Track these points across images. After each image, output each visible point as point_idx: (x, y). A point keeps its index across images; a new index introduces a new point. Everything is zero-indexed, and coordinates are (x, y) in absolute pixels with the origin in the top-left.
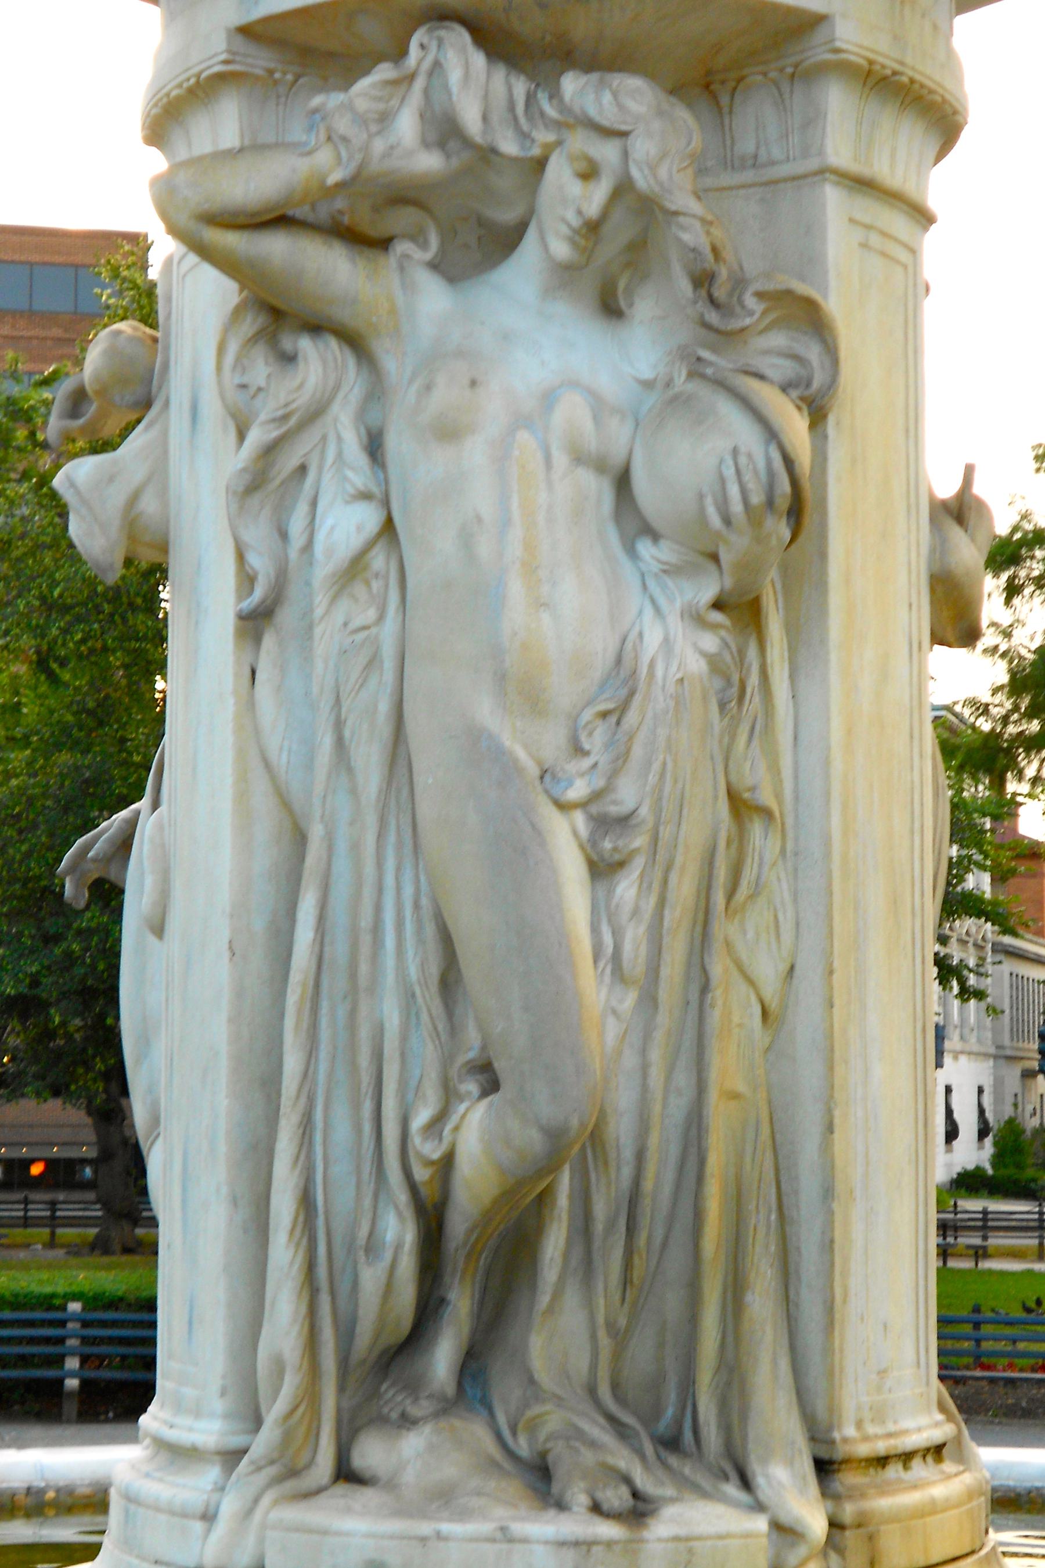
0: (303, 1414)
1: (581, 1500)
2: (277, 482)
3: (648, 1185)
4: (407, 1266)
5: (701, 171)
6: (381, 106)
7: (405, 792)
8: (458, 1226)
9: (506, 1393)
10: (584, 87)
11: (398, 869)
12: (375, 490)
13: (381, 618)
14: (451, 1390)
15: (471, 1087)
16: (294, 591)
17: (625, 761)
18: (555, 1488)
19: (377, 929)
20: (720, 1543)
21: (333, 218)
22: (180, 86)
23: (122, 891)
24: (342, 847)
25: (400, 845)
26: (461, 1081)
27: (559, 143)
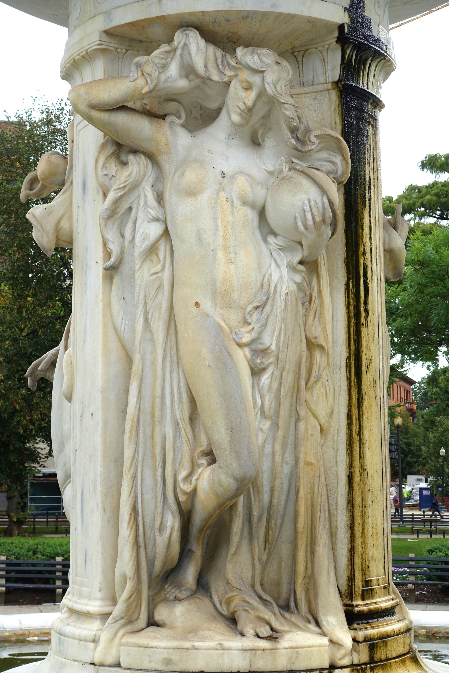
0: (135, 598)
1: (250, 631)
2: (120, 214)
3: (275, 501)
4: (176, 536)
5: (292, 87)
6: (163, 61)
7: (174, 339)
8: (198, 519)
9: (217, 588)
10: (246, 53)
11: (171, 372)
12: (162, 218)
13: (163, 269)
14: (194, 587)
15: (203, 461)
16: (127, 258)
17: (265, 327)
18: (240, 627)
19: (163, 397)
20: (309, 649)
21: (143, 107)
22: (79, 55)
23: (52, 384)
24: (148, 363)
25: (171, 363)
26: (199, 459)
27: (236, 75)
